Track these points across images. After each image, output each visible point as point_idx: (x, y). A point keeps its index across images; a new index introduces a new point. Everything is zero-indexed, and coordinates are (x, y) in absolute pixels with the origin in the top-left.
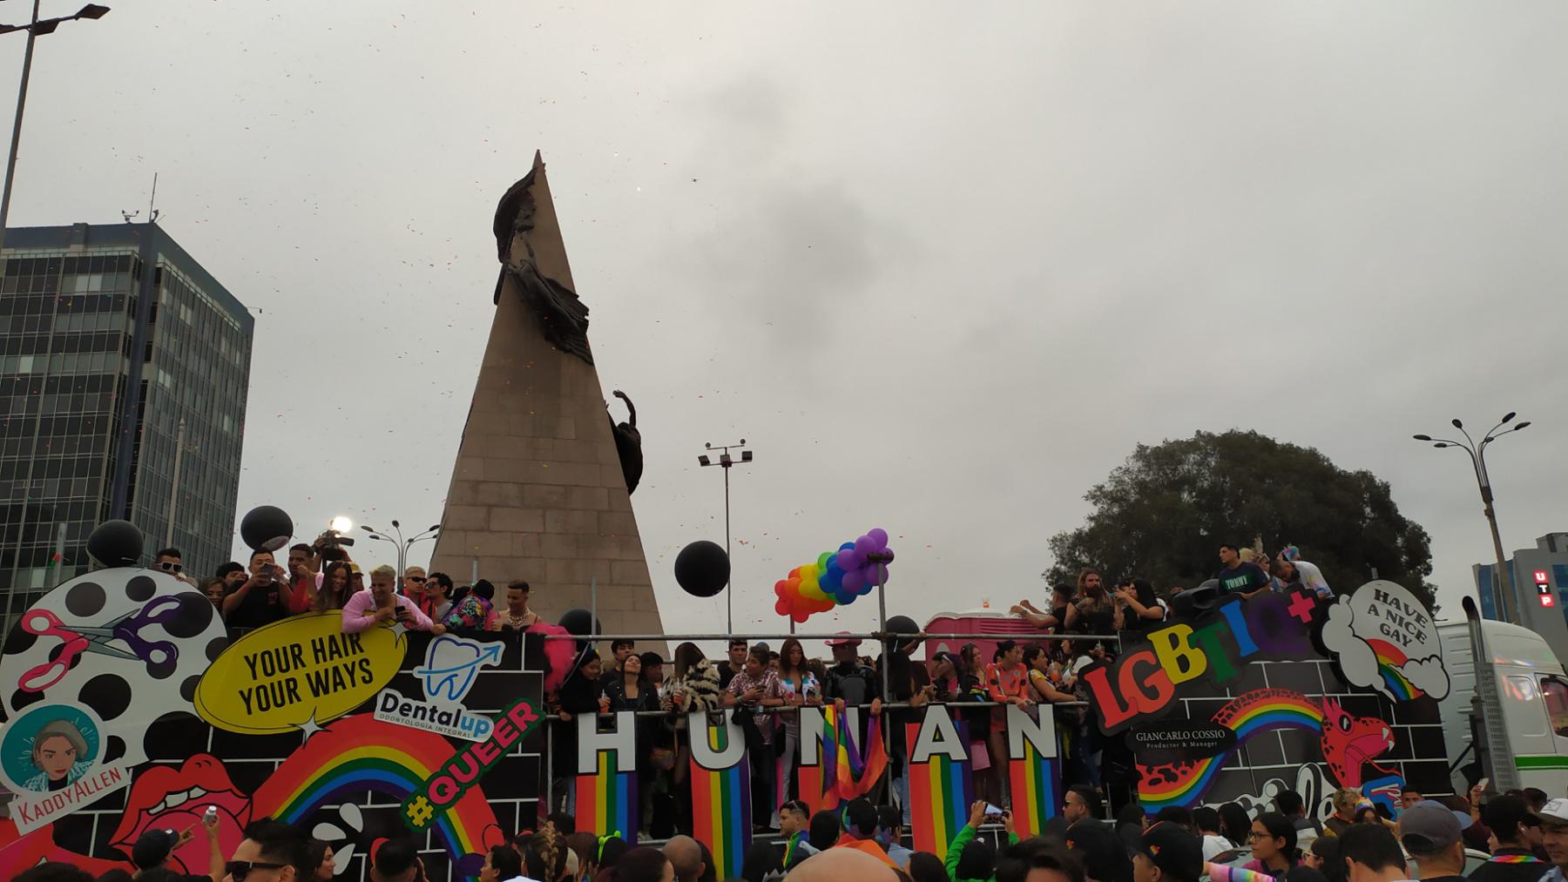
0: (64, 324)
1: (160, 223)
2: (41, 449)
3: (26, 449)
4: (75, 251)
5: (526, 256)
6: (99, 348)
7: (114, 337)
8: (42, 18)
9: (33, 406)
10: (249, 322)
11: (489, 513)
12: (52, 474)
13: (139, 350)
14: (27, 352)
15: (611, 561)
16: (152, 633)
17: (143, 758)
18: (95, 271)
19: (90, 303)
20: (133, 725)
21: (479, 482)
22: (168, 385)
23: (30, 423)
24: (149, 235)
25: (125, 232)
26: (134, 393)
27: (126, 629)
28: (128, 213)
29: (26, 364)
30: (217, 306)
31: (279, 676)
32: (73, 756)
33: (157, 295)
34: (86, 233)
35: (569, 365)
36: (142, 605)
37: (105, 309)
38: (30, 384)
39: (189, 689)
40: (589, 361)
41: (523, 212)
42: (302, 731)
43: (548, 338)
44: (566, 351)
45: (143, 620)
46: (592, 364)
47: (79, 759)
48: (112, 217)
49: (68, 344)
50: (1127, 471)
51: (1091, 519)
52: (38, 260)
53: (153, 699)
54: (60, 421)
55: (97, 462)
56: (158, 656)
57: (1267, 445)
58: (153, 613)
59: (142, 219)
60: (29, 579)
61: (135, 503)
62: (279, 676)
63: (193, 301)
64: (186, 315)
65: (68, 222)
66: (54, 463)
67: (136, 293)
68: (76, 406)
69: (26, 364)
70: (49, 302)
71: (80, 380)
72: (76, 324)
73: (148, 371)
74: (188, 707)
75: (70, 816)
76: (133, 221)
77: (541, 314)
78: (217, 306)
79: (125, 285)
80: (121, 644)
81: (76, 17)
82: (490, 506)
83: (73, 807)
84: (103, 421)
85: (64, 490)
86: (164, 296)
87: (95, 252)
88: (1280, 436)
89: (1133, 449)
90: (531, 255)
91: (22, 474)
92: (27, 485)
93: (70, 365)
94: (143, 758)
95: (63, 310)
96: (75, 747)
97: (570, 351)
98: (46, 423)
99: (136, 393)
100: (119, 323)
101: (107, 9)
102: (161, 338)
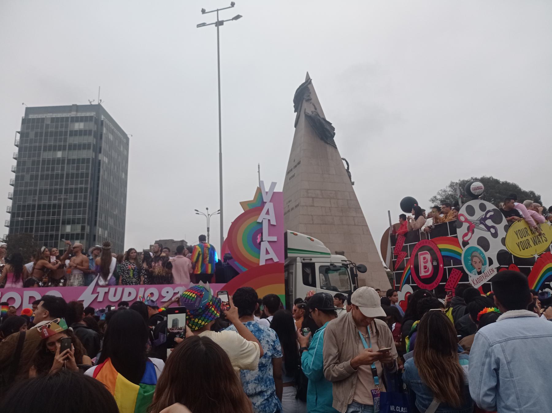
0: (72, 140)
1: (103, 105)
2: (67, 184)
3: (61, 184)
4: (73, 114)
5: (314, 110)
6: (84, 148)
7: (89, 145)
8: (220, 20)
9: (63, 169)
10: (128, 139)
11: (313, 200)
12: (71, 193)
13: (98, 150)
14: (60, 150)
15: (354, 217)
16: (489, 222)
17: (498, 265)
18: (81, 121)
19: (80, 133)
20: (493, 253)
21: (308, 190)
22: (107, 161)
23: (62, 175)
24: (98, 108)
25: (91, 107)
26: (97, 164)
27: (483, 221)
28: (91, 100)
29: (59, 154)
30: (120, 134)
31: (524, 239)
32: (481, 264)
33: (102, 130)
34: (77, 108)
35: (330, 149)
36: (484, 213)
37: (85, 134)
38: (61, 161)
39: (503, 241)
40: (335, 147)
41: (304, 95)
42: (534, 257)
43: (322, 139)
44: (328, 144)
45: (485, 219)
46: (336, 148)
47: (483, 265)
48: (85, 102)
49: (73, 147)
50: (445, 191)
51: (431, 208)
52: (61, 118)
53: (496, 246)
54: (73, 174)
55: (86, 189)
56: (493, 231)
57: (497, 182)
58: (488, 216)
59: (96, 103)
60: (65, 229)
61: (99, 202)
62: (524, 239)
63: (113, 133)
64: (111, 137)
65: (70, 104)
66: (71, 189)
67: (96, 129)
68: (78, 169)
69: (59, 154)
70: (66, 132)
71: (78, 160)
72: (76, 140)
73: (101, 157)
74: (504, 248)
75: (485, 284)
76: (93, 103)
77: (316, 130)
78: (120, 134)
79: (92, 126)
80: (482, 226)
81: (233, 19)
82: (313, 198)
83: (485, 281)
84: (87, 174)
85: (76, 198)
86: (105, 131)
87: (79, 115)
88: (502, 180)
89: (449, 183)
90: (316, 109)
91: (61, 192)
92: (63, 196)
93: (75, 155)
94: (498, 265)
95: (71, 135)
96: (481, 261)
97: (329, 144)
98: (68, 175)
99: (97, 165)
100: (90, 139)
101: (241, 16)
102: (104, 145)
